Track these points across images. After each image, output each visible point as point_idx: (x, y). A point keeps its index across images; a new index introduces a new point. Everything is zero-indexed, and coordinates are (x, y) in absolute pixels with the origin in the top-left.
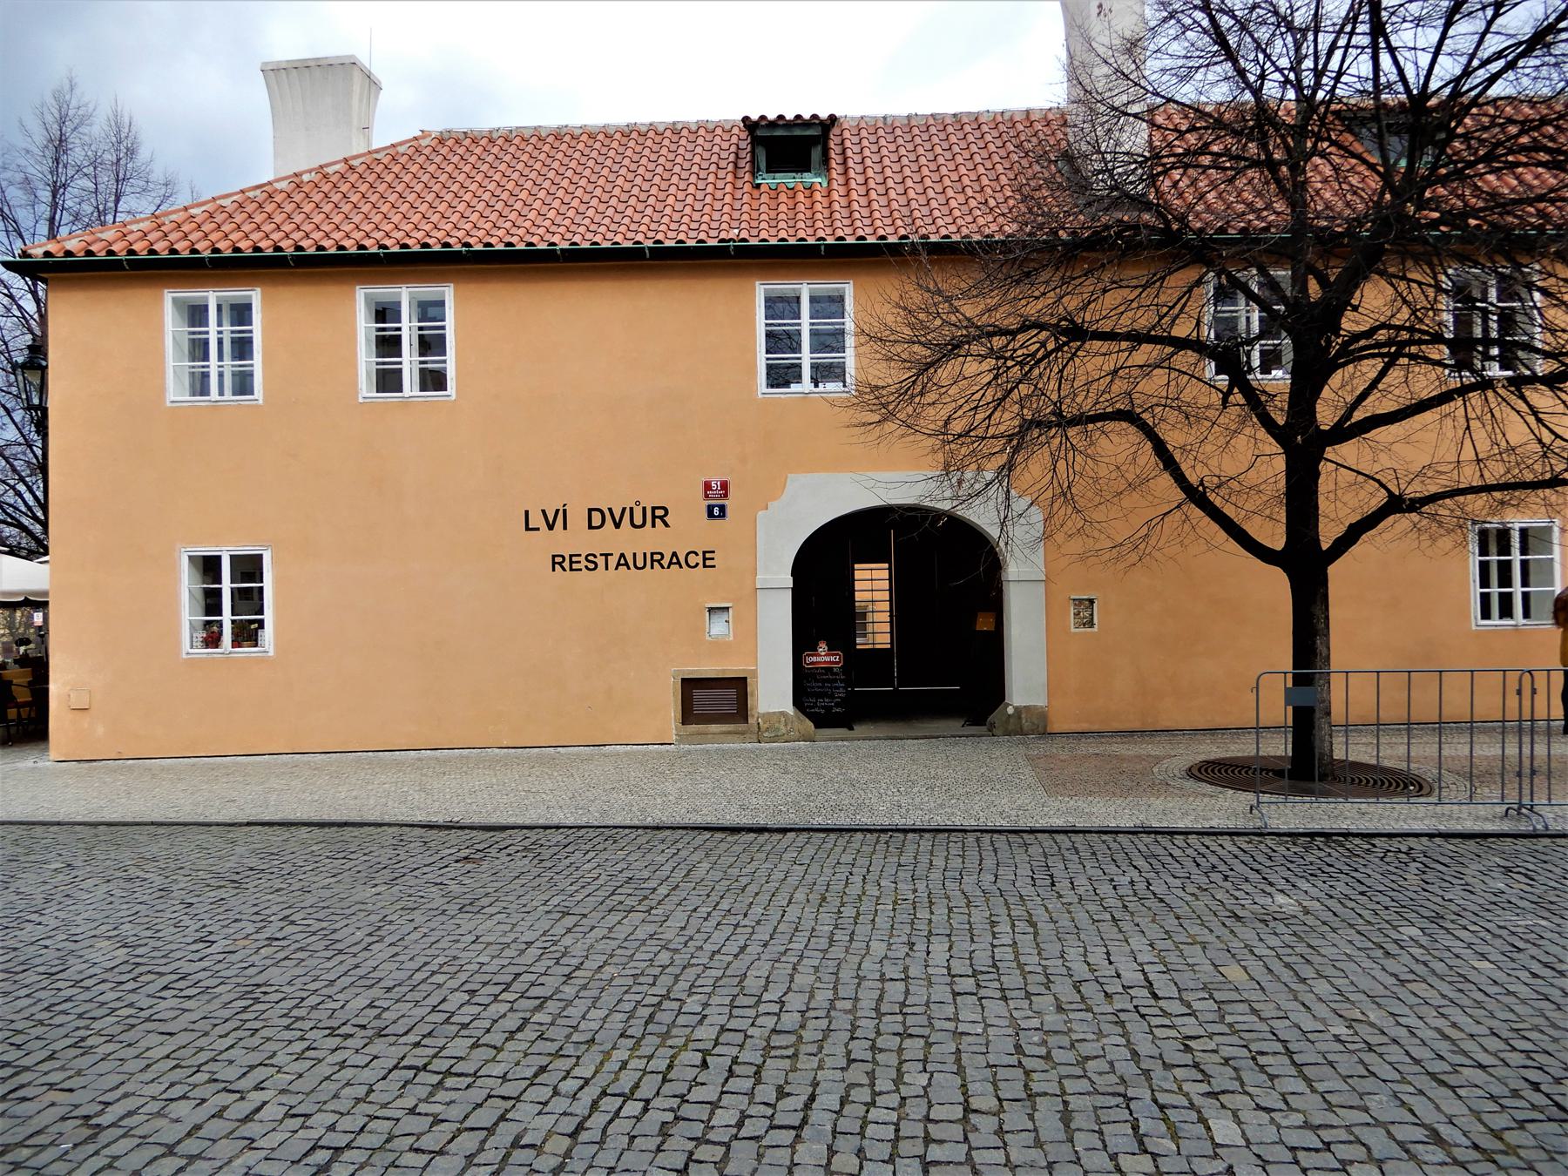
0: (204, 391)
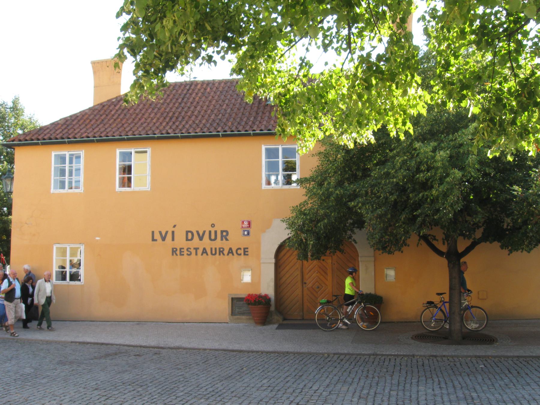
0: (63, 187)
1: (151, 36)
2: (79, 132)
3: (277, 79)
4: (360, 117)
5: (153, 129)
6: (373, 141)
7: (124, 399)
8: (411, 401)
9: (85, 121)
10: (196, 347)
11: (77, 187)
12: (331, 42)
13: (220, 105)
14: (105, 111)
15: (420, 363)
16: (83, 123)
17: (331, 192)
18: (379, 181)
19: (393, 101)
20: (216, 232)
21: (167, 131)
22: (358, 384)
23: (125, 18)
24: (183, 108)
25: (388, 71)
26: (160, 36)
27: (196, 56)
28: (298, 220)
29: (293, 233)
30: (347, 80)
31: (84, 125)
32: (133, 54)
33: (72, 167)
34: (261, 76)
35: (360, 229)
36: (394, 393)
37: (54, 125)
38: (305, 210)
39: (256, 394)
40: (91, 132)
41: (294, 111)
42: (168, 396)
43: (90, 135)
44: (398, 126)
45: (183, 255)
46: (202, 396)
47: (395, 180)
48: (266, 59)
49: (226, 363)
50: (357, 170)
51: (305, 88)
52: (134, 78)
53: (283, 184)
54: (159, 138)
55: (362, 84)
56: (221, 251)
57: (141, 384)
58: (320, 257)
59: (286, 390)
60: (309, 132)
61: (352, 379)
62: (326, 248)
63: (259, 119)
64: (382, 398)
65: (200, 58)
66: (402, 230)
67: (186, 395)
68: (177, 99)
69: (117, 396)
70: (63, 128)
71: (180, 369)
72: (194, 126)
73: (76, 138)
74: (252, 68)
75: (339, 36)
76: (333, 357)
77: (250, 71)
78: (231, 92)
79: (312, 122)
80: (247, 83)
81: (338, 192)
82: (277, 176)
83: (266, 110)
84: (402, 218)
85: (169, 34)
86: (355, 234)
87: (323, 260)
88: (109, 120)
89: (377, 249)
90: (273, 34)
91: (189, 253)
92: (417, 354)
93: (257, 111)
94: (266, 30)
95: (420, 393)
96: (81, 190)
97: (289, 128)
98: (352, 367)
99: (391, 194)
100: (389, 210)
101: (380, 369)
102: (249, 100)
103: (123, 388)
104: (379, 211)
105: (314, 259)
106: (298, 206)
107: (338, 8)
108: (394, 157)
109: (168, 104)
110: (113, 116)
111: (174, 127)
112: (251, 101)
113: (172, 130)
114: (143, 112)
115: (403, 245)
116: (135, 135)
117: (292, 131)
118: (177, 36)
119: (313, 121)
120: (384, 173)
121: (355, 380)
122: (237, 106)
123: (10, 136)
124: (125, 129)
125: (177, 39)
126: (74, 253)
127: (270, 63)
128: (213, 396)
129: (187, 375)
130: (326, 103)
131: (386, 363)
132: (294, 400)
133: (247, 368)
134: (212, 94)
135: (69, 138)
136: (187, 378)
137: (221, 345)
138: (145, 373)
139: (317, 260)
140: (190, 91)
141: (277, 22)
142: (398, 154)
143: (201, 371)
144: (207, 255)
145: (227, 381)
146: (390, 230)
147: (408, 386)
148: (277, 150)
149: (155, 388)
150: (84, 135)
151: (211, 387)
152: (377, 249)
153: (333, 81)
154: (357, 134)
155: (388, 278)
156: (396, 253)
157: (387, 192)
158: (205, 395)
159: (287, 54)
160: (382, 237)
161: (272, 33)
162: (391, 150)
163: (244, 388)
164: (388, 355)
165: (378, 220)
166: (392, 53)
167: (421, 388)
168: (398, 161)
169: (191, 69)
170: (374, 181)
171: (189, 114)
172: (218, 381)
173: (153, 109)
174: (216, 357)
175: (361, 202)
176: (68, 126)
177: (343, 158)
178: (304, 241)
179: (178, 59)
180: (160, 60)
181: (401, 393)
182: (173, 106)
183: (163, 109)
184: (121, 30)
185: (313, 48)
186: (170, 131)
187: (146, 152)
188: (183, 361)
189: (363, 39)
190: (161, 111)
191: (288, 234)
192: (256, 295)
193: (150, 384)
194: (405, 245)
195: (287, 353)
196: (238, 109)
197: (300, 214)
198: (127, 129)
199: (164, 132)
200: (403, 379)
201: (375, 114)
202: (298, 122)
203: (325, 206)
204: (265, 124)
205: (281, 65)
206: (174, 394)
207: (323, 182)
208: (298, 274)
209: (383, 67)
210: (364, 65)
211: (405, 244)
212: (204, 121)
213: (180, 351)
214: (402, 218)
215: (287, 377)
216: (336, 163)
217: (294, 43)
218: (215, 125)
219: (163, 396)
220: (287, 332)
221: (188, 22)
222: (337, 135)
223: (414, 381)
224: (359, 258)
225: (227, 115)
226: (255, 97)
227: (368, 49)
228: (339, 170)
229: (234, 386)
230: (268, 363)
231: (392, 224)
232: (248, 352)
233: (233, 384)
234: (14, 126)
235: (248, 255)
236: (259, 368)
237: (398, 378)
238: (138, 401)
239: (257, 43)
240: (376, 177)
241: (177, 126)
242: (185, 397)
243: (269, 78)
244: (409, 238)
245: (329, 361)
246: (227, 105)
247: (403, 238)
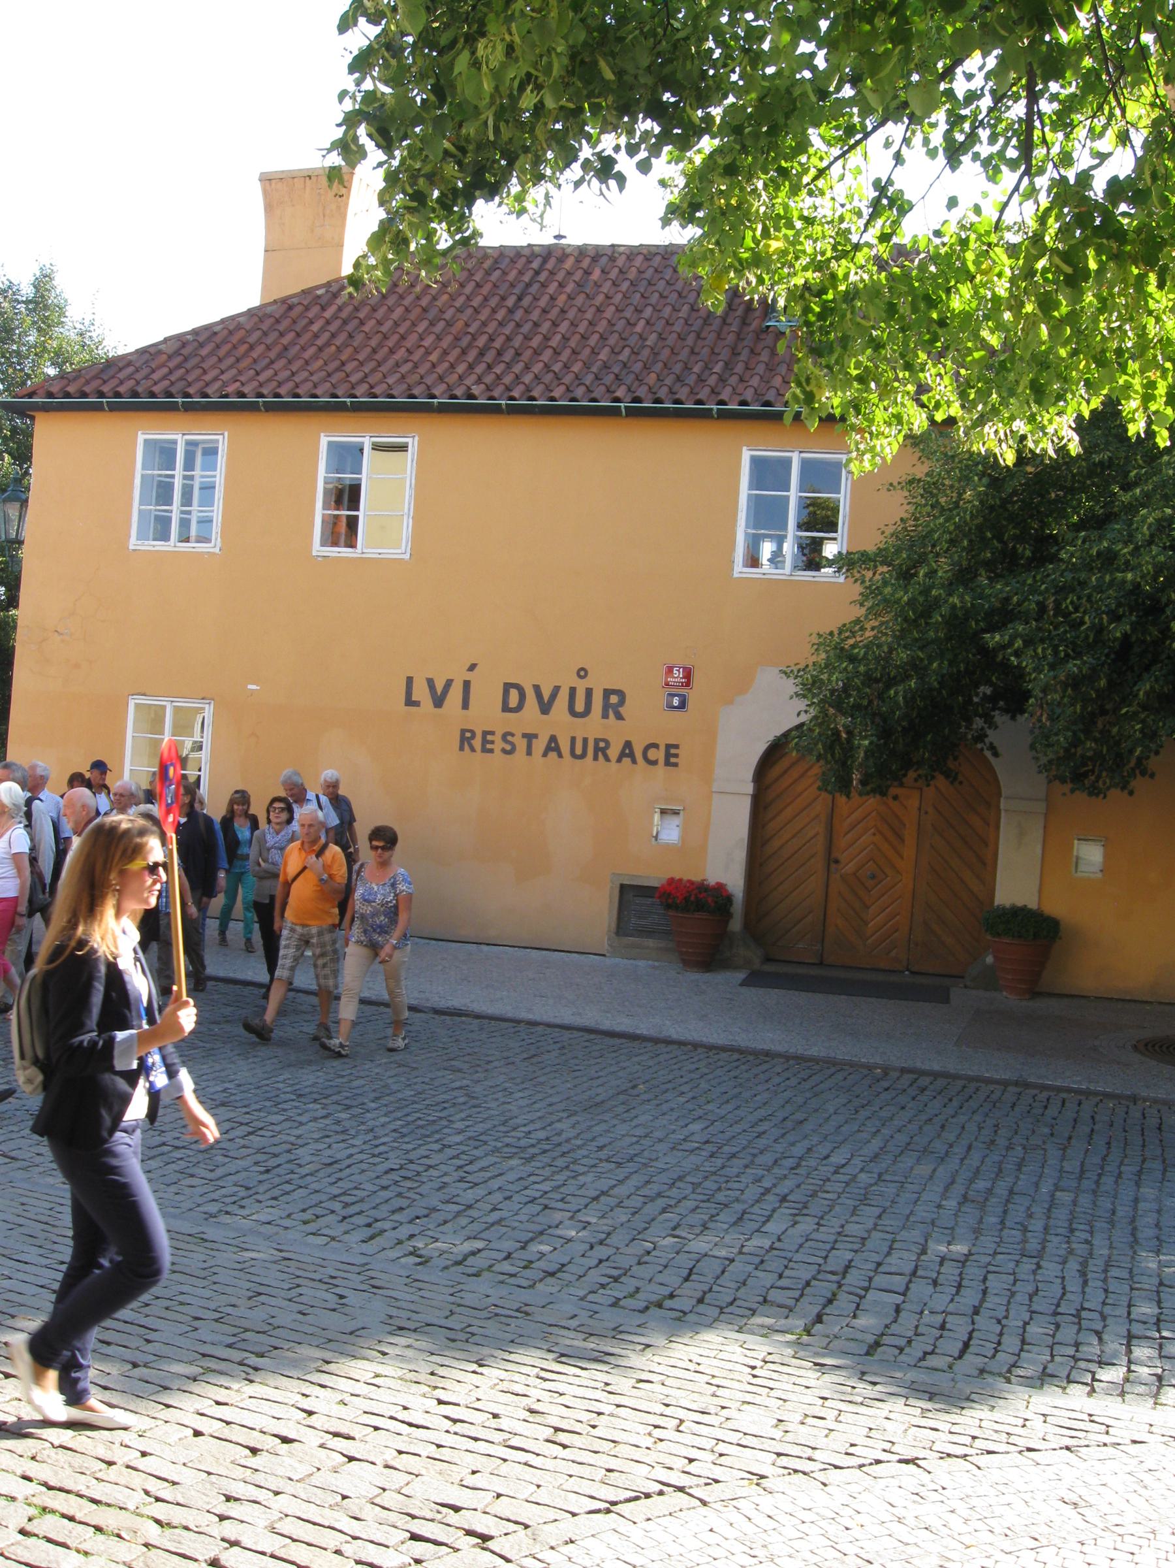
0: (164, 536)
1: (440, 93)
2: (216, 379)
3: (801, 243)
4: (1040, 371)
5: (429, 380)
6: (1074, 448)
7: (299, 1137)
8: (1112, 1223)
9: (235, 347)
10: (510, 1015)
11: (204, 539)
12: (972, 137)
13: (629, 323)
14: (294, 322)
15: (1153, 1122)
16: (228, 354)
17: (937, 599)
18: (1083, 576)
19: (1145, 327)
20: (589, 693)
21: (469, 388)
22: (962, 1160)
23: (365, 32)
24: (518, 325)
25: (1138, 231)
26: (465, 90)
27: (567, 157)
28: (830, 675)
29: (813, 712)
30: (1010, 257)
31: (231, 360)
32: (384, 143)
33: (192, 478)
34: (754, 230)
35: (1013, 718)
36: (1065, 1197)
37: (147, 356)
38: (853, 646)
39: (668, 1159)
40: (251, 380)
41: (845, 341)
42: (421, 1142)
43: (246, 390)
44: (1153, 407)
45: (491, 751)
46: (514, 1150)
47: (1129, 576)
48: (771, 180)
49: (590, 1065)
50: (1017, 538)
51: (883, 274)
52: (382, 214)
53: (795, 567)
54: (443, 409)
55: (1057, 267)
56: (601, 749)
57: (347, 1102)
58: (888, 787)
59: (755, 1156)
60: (886, 409)
61: (946, 1146)
62: (907, 763)
63: (739, 368)
64: (1028, 1208)
65: (576, 167)
66: (1138, 727)
67: (471, 1142)
68: (503, 299)
69: (277, 1128)
70: (171, 365)
71: (460, 1070)
72: (548, 378)
73: (207, 396)
74: (728, 204)
75: (999, 120)
76: (898, 1079)
77: (723, 213)
78: (661, 285)
79: (897, 379)
80: (712, 251)
81: (955, 600)
82: (780, 541)
83: (761, 345)
84: (1141, 693)
85: (493, 85)
86: (996, 727)
87: (895, 798)
88: (303, 349)
89: (1056, 777)
90: (799, 105)
91: (508, 747)
92: (1144, 1094)
93: (736, 345)
94: (777, 89)
95: (1142, 1205)
96: (214, 546)
97: (827, 394)
98: (950, 1111)
99: (1116, 617)
100: (1103, 665)
101: (1031, 1126)
102: (714, 302)
103: (296, 1107)
104: (1075, 665)
105: (868, 793)
106: (836, 632)
107: (1004, 27)
108: (1132, 509)
109: (477, 311)
110: (316, 336)
111: (489, 379)
112: (718, 306)
113: (483, 387)
114: (402, 330)
115: (1137, 772)
116: (376, 397)
117: (836, 401)
118: (515, 93)
119: (901, 375)
120: (1099, 554)
121: (955, 1150)
122: (677, 328)
123: (24, 383)
124: (348, 376)
125: (514, 99)
126: (183, 725)
127: (782, 194)
128: (545, 1152)
129: (478, 1089)
130: (942, 323)
131: (1052, 1111)
132: (775, 1185)
133: (647, 1085)
134: (606, 287)
135: (187, 395)
136: (477, 1098)
137: (580, 1014)
138: (362, 1074)
139: (878, 796)
140: (542, 277)
141: (814, 69)
142: (1146, 500)
143: (519, 1080)
144: (560, 756)
145: (590, 1116)
146: (1100, 725)
147: (1108, 1181)
148: (787, 463)
149: (385, 1115)
150: (230, 389)
151: (543, 1128)
152: (1056, 777)
153: (970, 256)
154: (1029, 423)
155: (1081, 867)
156: (1115, 793)
157: (1103, 612)
158: (523, 1149)
159: (836, 169)
160: (1076, 743)
161: (794, 101)
162: (1126, 487)
163: (635, 1139)
164: (1059, 1089)
165: (1069, 691)
166: (1154, 176)
167: (1147, 1191)
168: (1144, 520)
169: (547, 197)
170: (1069, 576)
171: (536, 342)
172: (565, 1115)
173: (432, 324)
174: (563, 1047)
175: (1021, 636)
176: (186, 359)
177: (981, 502)
178: (844, 735)
179: (511, 164)
180: (460, 163)
181: (1085, 1200)
182: (490, 318)
183: (460, 324)
184: (352, 69)
185: (915, 155)
186: (476, 390)
187: (403, 448)
188: (470, 1051)
189: (1071, 132)
190: (454, 330)
191: (799, 714)
192: (691, 882)
193: (373, 1105)
194: (1143, 774)
195: (767, 1054)
196: (679, 335)
197: (839, 658)
198: (354, 379)
199: (459, 392)
200: (1097, 1160)
201: (1087, 366)
202: (854, 373)
203: (916, 640)
204: (755, 385)
205: (818, 201)
206: (437, 1136)
207: (915, 567)
208: (817, 834)
209: (1125, 221)
210: (1066, 210)
211: (1141, 769)
212: (576, 368)
213: (463, 1022)
214: (1141, 693)
215: (761, 1120)
216: (958, 515)
217: (858, 137)
218: (609, 379)
219: (406, 1139)
220: (773, 997)
221: (549, 51)
222: (969, 423)
223: (1129, 1170)
224: (1002, 800)
225: (646, 353)
226: (734, 293)
227: (1084, 161)
228: (965, 536)
229: (608, 1131)
230: (710, 1076)
231: (1108, 707)
232: (656, 1041)
233: (604, 1126)
234: (36, 354)
235: (676, 765)
236: (683, 1089)
237: (1082, 1156)
238: (335, 1146)
239: (747, 130)
240: (1073, 564)
241: (498, 377)
242: (466, 1148)
243: (777, 239)
244: (1157, 753)
245: (886, 1089)
246: (648, 323)
247: (1139, 750)
